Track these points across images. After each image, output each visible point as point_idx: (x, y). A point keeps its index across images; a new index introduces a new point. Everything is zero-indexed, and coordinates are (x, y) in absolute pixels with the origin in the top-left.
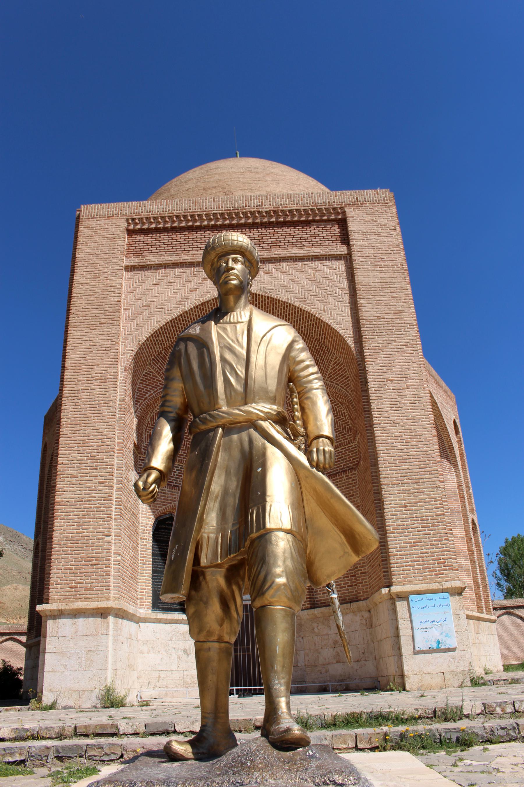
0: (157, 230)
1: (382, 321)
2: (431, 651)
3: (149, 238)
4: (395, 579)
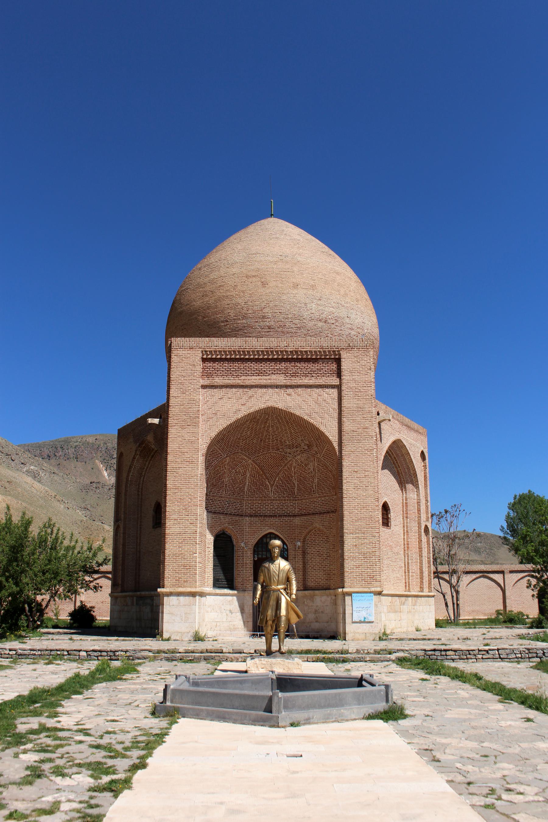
0: (221, 360)
1: (355, 434)
2: (360, 622)
3: (216, 365)
4: (346, 585)
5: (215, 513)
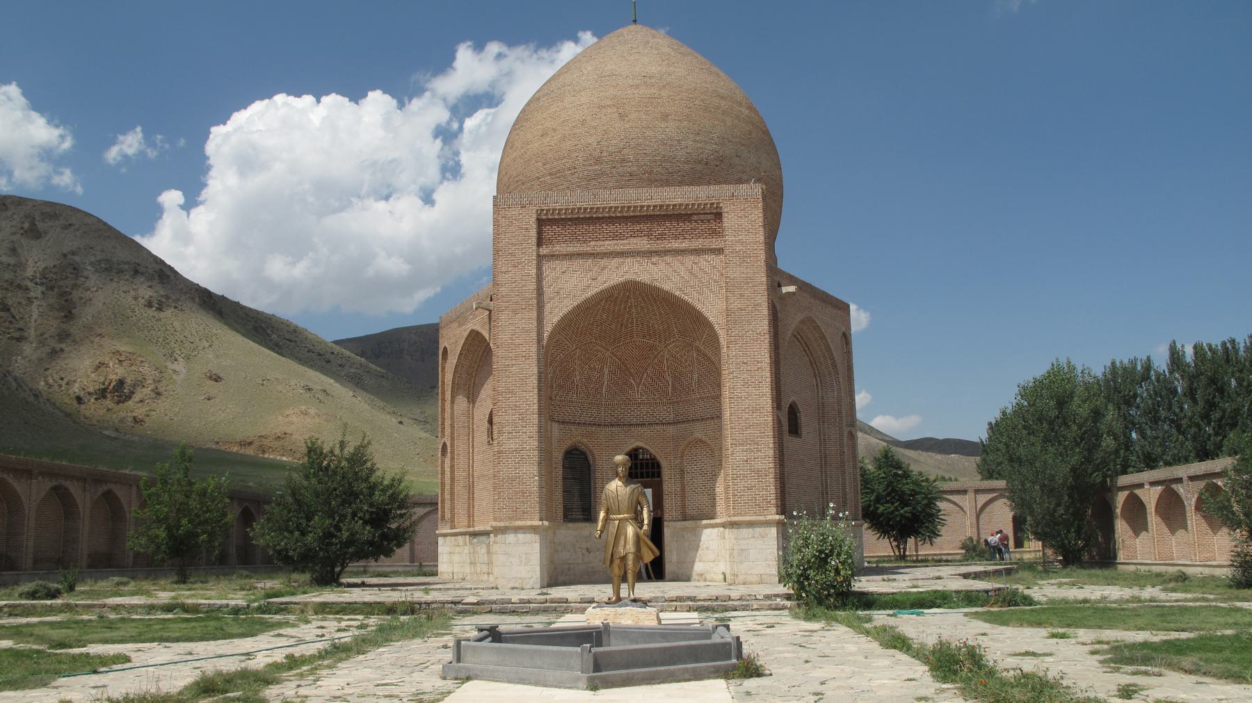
5: (563, 423)
